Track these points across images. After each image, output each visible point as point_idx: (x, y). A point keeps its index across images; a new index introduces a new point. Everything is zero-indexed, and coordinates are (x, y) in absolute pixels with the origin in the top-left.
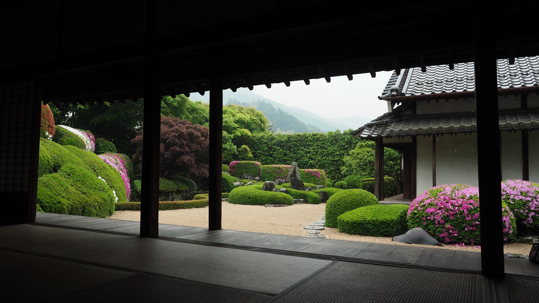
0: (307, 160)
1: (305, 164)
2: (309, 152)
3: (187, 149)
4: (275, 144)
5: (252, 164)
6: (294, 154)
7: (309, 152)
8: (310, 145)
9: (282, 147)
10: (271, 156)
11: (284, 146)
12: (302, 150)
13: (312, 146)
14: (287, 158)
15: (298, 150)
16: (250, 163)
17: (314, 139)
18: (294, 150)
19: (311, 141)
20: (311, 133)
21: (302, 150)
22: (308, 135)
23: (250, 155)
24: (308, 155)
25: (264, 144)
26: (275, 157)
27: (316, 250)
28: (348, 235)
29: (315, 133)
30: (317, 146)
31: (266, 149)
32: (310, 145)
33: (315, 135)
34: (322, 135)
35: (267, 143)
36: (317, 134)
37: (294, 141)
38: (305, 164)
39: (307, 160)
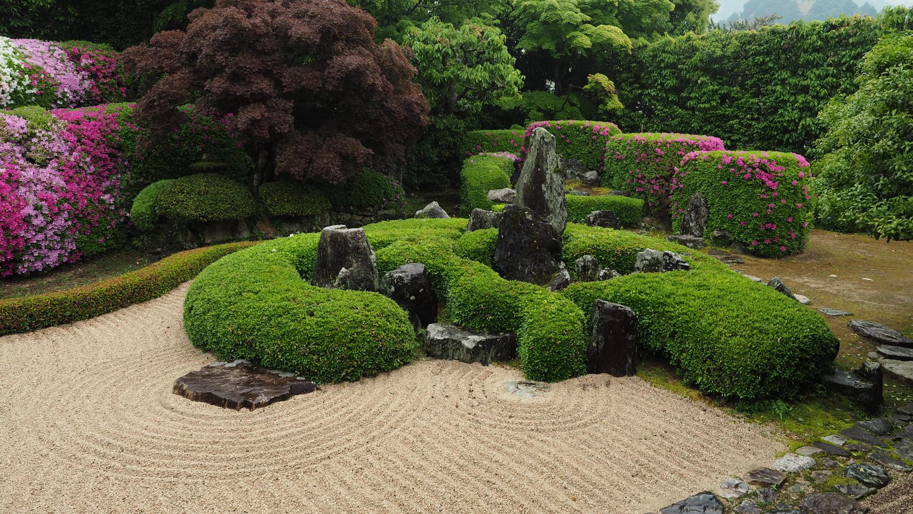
0: (796, 114)
1: (786, 131)
2: (805, 90)
3: (264, 85)
4: (696, 68)
5: (584, 131)
6: (755, 95)
7: (805, 90)
8: (809, 65)
9: (715, 75)
10: (682, 104)
11: (722, 72)
12: (783, 82)
13: (818, 66)
14: (729, 111)
15: (768, 83)
16: (576, 128)
17: (826, 40)
18: (755, 85)
19: (817, 50)
20: (822, 22)
21: (783, 82)
22: (804, 31)
23: (615, 103)
24: (801, 98)
25: (666, 67)
26: (693, 109)
27: (368, 399)
28: (382, 377)
29: (834, 21)
30: (837, 65)
31: (671, 82)
32: (809, 65)
33: (833, 27)
34: (858, 24)
35: (673, 66)
36: (842, 24)
37: (758, 53)
38: (786, 131)
39: (796, 114)
